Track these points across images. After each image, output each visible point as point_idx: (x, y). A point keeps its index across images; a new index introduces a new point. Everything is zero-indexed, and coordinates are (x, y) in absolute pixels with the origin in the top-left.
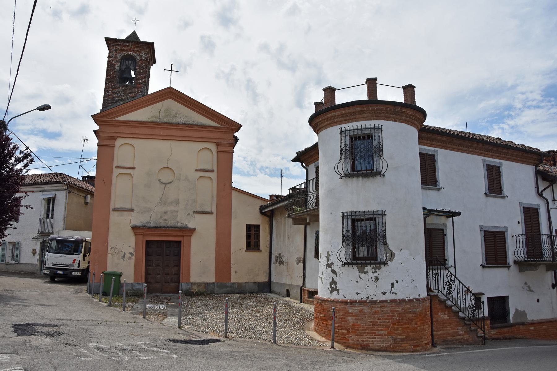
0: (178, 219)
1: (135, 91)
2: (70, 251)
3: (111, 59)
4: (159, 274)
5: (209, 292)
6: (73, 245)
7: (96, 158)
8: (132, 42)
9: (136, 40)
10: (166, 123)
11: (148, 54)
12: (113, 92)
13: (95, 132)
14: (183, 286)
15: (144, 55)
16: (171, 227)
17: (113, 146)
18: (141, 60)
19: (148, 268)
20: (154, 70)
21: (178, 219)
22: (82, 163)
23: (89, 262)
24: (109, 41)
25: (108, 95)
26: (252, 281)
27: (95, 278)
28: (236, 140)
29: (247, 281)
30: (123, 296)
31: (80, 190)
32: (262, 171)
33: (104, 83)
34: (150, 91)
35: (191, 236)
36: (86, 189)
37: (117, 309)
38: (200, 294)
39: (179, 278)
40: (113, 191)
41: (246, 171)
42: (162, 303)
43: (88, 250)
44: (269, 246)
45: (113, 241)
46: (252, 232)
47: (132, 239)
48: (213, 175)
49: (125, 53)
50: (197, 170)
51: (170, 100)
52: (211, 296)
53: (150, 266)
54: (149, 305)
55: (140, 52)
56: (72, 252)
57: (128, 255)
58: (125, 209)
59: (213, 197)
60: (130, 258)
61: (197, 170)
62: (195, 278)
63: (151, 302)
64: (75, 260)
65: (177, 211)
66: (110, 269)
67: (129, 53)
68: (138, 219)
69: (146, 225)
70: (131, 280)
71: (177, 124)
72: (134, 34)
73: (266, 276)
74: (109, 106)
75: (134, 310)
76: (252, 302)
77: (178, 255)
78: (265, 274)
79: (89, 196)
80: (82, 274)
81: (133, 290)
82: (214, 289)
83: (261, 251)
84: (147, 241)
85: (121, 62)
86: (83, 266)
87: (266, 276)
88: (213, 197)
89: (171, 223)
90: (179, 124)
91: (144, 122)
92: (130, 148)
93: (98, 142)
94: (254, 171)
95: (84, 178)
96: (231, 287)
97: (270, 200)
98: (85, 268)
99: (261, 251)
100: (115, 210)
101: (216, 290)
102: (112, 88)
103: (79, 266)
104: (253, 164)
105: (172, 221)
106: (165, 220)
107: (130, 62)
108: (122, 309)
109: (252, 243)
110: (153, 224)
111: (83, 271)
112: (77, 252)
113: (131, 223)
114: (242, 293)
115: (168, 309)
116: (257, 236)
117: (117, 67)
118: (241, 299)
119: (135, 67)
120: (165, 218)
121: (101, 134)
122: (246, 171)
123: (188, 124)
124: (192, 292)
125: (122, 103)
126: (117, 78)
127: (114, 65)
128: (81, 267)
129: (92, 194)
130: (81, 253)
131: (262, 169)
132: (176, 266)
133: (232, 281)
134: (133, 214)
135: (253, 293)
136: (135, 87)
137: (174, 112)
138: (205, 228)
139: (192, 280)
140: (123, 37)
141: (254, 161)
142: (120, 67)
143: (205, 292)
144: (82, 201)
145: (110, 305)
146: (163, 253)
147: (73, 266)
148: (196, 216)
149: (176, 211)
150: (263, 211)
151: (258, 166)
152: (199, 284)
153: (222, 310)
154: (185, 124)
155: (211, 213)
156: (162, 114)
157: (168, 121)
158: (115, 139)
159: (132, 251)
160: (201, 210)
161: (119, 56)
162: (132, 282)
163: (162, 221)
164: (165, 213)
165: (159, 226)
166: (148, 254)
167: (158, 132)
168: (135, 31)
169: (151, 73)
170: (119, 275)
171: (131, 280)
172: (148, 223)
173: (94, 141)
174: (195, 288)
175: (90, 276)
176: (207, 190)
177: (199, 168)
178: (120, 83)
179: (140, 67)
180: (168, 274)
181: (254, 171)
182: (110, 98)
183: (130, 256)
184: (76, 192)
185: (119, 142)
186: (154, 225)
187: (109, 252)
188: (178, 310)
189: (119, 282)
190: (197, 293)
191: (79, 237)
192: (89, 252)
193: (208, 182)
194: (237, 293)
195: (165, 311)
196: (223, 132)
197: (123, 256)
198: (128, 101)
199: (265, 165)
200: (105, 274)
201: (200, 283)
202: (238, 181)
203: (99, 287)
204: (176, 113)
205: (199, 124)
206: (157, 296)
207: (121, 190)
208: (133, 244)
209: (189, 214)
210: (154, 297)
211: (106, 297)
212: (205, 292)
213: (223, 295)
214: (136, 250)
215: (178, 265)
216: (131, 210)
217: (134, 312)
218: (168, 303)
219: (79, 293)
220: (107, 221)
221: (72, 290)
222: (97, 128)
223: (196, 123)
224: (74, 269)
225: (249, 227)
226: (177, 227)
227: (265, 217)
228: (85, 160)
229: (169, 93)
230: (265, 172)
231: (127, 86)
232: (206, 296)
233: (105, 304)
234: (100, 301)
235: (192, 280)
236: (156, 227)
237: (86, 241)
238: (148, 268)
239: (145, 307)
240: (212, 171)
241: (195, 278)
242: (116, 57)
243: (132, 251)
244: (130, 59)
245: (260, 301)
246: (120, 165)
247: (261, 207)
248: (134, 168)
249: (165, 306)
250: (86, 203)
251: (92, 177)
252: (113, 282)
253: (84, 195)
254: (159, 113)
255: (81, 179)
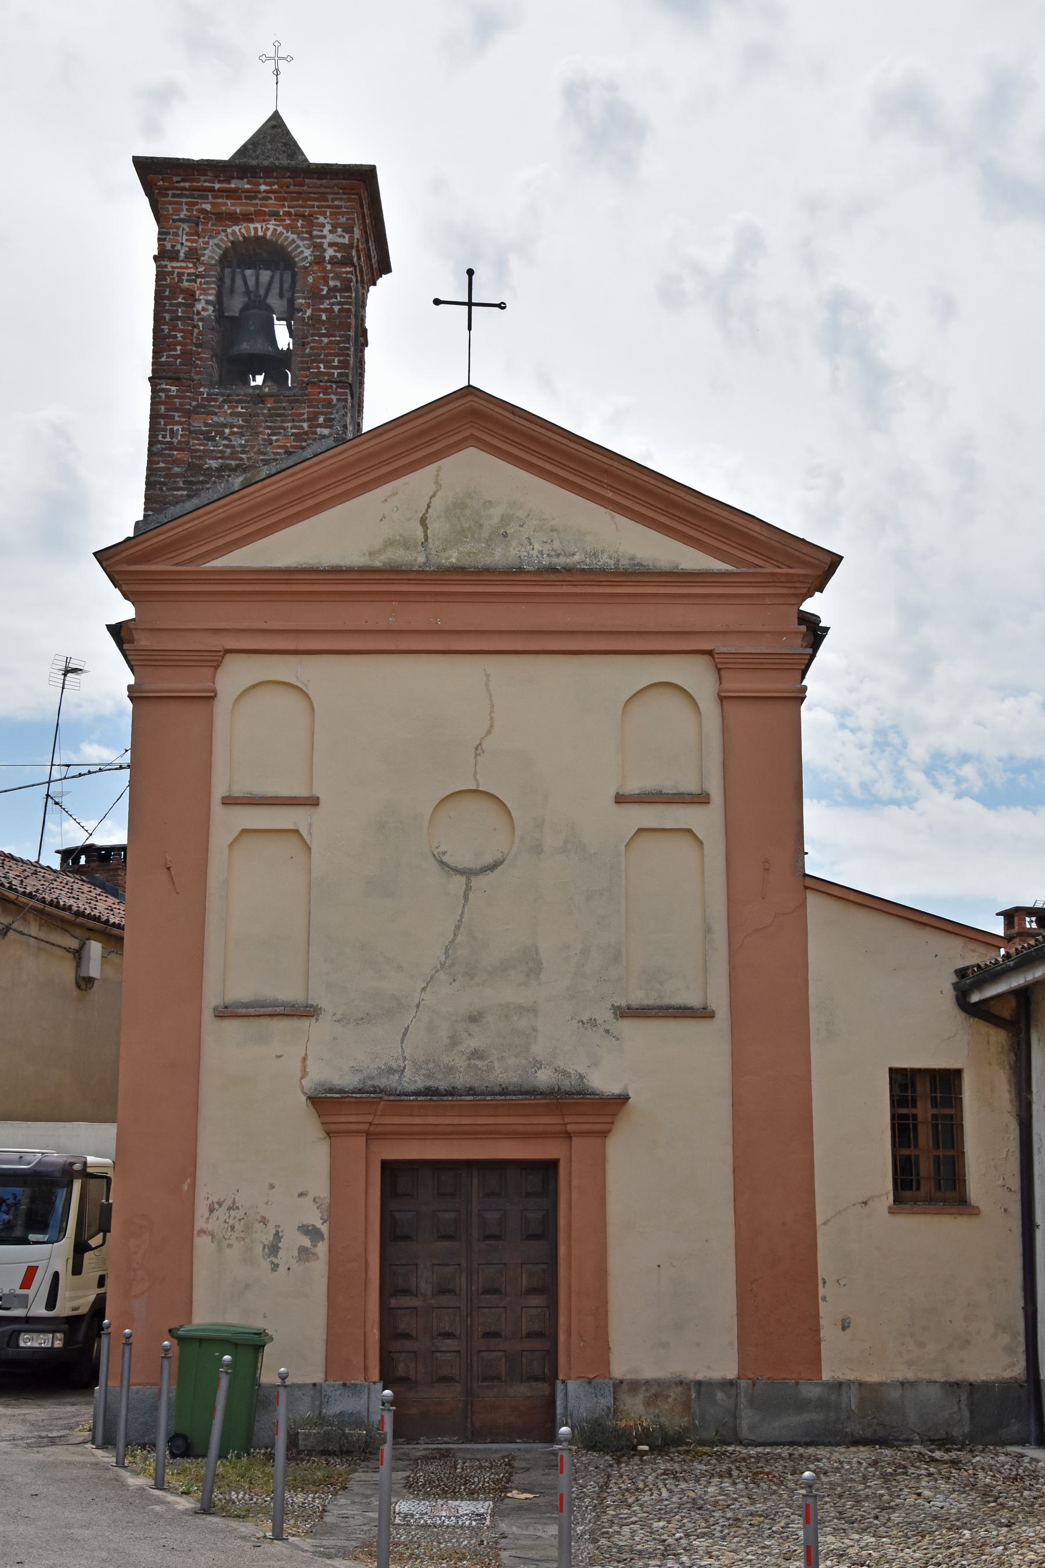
0: (539, 1049)
1: (297, 418)
2: (9, 1226)
3: (170, 265)
4: (450, 1335)
5: (710, 1434)
6: (23, 1193)
7: (127, 759)
8: (268, 172)
9: (284, 161)
10: (459, 572)
11: (348, 230)
12: (191, 432)
13: (117, 631)
14: (575, 1398)
15: (329, 236)
16: (505, 1092)
17: (209, 698)
18: (319, 260)
19: (394, 1302)
20: (381, 302)
21: (539, 1049)
22: (55, 788)
23: (102, 1281)
24: (159, 176)
25: (170, 446)
26: (938, 1376)
27: (134, 1364)
28: (814, 632)
29: (910, 1376)
30: (270, 1457)
31: (54, 916)
32: (942, 778)
33: (144, 393)
34: (373, 417)
35: (604, 1134)
36: (79, 914)
37: (246, 1528)
38: (665, 1443)
39: (552, 1354)
40: (213, 919)
41: (854, 782)
42: (472, 1495)
43: (99, 1219)
44: (1015, 1184)
45: (224, 1169)
46: (924, 1111)
47: (316, 1156)
48: (707, 821)
49: (238, 230)
50: (621, 799)
51: (471, 454)
52: (720, 1457)
53: (407, 1292)
54: (403, 1506)
55: (309, 220)
56: (18, 1232)
57: (293, 1240)
58: (275, 1004)
59: (708, 930)
60: (305, 1254)
61: (621, 799)
62: (633, 1355)
63: (411, 1488)
64: (31, 1272)
65: (533, 1010)
66: (205, 1315)
67: (256, 228)
68: (339, 1057)
69: (383, 1082)
70: (310, 1370)
71: (514, 573)
72: (275, 131)
73: (1009, 1350)
74: (178, 501)
75: (330, 1531)
76: (941, 1497)
77: (545, 1232)
78: (1005, 1339)
79: (95, 948)
80: (67, 1342)
81: (322, 1420)
82: (735, 1415)
83: (975, 1212)
84: (385, 1164)
85: (221, 280)
86: (75, 1300)
87: (1009, 1350)
88: (708, 930)
89: (504, 1072)
90: (520, 571)
91: (349, 570)
92: (287, 701)
93: (131, 680)
94: (899, 778)
95: (68, 855)
96: (822, 1404)
97: (1008, 939)
98: (84, 1310)
99: (975, 1212)
100: (225, 1013)
101: (747, 1420)
102: (188, 414)
103: (51, 1304)
104: (887, 741)
105: (512, 1061)
106: (476, 1054)
107: (265, 275)
108: (267, 1528)
109: (926, 1167)
110: (413, 1080)
111: (71, 1323)
112: (41, 1226)
113: (304, 1074)
114: (884, 1443)
115: (503, 1526)
116: (950, 1132)
117: (204, 306)
118: (885, 1478)
119: (291, 301)
120: (473, 1044)
121: (144, 642)
122: (854, 782)
123: (569, 570)
124: (621, 1434)
125: (237, 481)
126: (207, 362)
127: (191, 295)
128: (63, 1308)
129: (111, 935)
130: (63, 1231)
131: (938, 766)
132: (532, 1291)
133: (826, 1376)
134: (317, 1030)
135: (944, 1442)
136: (294, 402)
137: (496, 514)
138: (676, 1089)
139: (619, 1369)
140: (223, 150)
141: (895, 728)
142: (219, 304)
143: (686, 1432)
144: (67, 971)
145: (207, 1509)
146: (467, 1211)
147: (24, 1302)
148: (628, 1027)
149: (523, 1010)
150: (975, 998)
151: (919, 751)
152: (655, 1390)
153: (783, 1535)
154: (552, 570)
155: (705, 1013)
156: (438, 527)
157: (467, 562)
158: (215, 660)
159: (315, 1218)
160: (651, 1000)
161: (211, 253)
162: (318, 1377)
163: (460, 1062)
164: (475, 1018)
165: (443, 1085)
166: (392, 1233)
167: (419, 616)
168: (276, 116)
169: (368, 324)
170: (251, 1346)
171: (310, 1370)
172: (391, 1071)
173: (112, 676)
174: (636, 1411)
175: (107, 1350)
176: (685, 886)
177: (633, 787)
178: (221, 383)
179: (315, 296)
180: (496, 1335)
181: (899, 778)
182: (177, 462)
183: (306, 1242)
184: (34, 929)
185: (234, 677)
186: (420, 1083)
187: (200, 1224)
188: (553, 1530)
189: (255, 1380)
190: (645, 1436)
191: (55, 1156)
192: (105, 1227)
193: (681, 849)
194: (855, 1443)
195: (487, 1537)
196: (749, 594)
197: (267, 1248)
198: (265, 471)
199: (951, 743)
200: (182, 1340)
201: (659, 1383)
202: (836, 845)
203: (156, 1409)
204: (506, 519)
205: (625, 563)
206: (445, 1454)
207: (252, 913)
208: (320, 1187)
209: (593, 1022)
210: (427, 1459)
211: (187, 1463)
212: (686, 1432)
213: (785, 1451)
214: (332, 1215)
215: (547, 1287)
216: (307, 1012)
217: (329, 1542)
218: (499, 1490)
219: (53, 1441)
220: (187, 1069)
221: (18, 1429)
222: (125, 611)
223: (605, 560)
224: (27, 1320)
225: (904, 1083)
226: (534, 1092)
227: (982, 1026)
228: (73, 771)
229: (470, 419)
230: (959, 780)
231: (259, 397)
232: (697, 1456)
233: (185, 1504)
234: (160, 1484)
235: (619, 1369)
236: (429, 1092)
237: (86, 1175)
238: (394, 1302)
239: (386, 1513)
240: (701, 799)
241: (633, 1355)
242: (193, 255)
243: (315, 1218)
244: (262, 257)
245: (986, 1493)
246: (240, 790)
247: (962, 973)
248: (313, 802)
249: (483, 1507)
250: (85, 983)
251: (109, 849)
252: (224, 1382)
253: (74, 944)
254: (423, 522)
255: (55, 862)
